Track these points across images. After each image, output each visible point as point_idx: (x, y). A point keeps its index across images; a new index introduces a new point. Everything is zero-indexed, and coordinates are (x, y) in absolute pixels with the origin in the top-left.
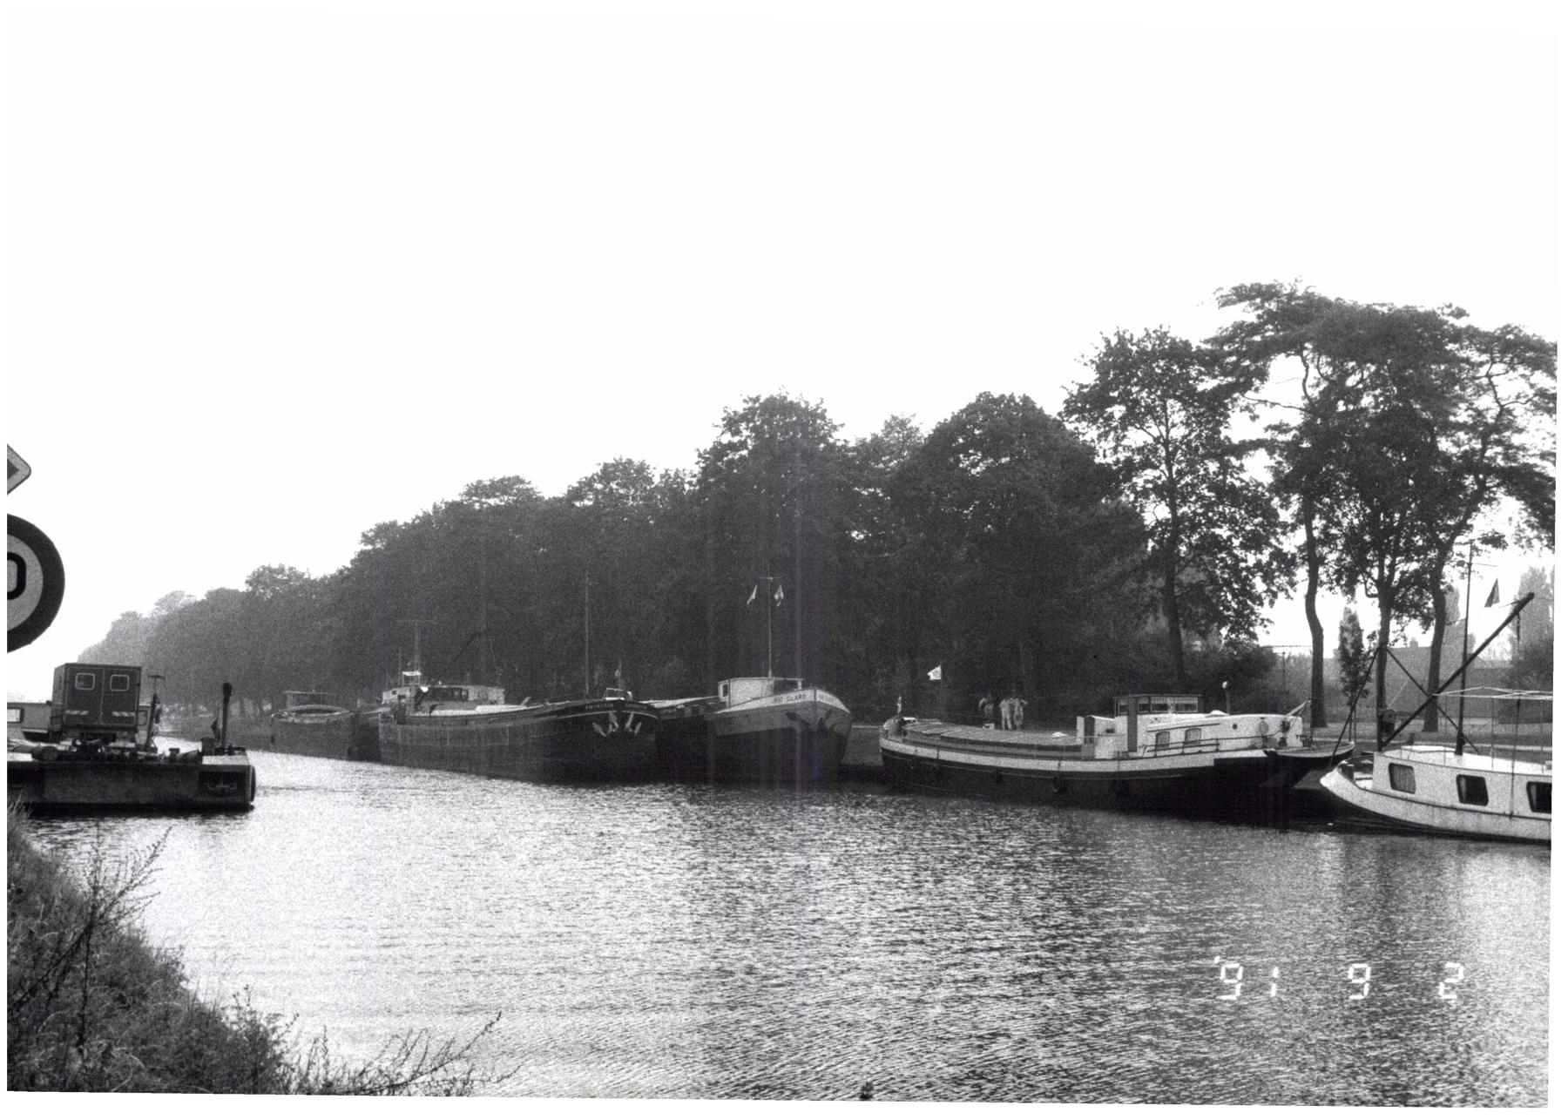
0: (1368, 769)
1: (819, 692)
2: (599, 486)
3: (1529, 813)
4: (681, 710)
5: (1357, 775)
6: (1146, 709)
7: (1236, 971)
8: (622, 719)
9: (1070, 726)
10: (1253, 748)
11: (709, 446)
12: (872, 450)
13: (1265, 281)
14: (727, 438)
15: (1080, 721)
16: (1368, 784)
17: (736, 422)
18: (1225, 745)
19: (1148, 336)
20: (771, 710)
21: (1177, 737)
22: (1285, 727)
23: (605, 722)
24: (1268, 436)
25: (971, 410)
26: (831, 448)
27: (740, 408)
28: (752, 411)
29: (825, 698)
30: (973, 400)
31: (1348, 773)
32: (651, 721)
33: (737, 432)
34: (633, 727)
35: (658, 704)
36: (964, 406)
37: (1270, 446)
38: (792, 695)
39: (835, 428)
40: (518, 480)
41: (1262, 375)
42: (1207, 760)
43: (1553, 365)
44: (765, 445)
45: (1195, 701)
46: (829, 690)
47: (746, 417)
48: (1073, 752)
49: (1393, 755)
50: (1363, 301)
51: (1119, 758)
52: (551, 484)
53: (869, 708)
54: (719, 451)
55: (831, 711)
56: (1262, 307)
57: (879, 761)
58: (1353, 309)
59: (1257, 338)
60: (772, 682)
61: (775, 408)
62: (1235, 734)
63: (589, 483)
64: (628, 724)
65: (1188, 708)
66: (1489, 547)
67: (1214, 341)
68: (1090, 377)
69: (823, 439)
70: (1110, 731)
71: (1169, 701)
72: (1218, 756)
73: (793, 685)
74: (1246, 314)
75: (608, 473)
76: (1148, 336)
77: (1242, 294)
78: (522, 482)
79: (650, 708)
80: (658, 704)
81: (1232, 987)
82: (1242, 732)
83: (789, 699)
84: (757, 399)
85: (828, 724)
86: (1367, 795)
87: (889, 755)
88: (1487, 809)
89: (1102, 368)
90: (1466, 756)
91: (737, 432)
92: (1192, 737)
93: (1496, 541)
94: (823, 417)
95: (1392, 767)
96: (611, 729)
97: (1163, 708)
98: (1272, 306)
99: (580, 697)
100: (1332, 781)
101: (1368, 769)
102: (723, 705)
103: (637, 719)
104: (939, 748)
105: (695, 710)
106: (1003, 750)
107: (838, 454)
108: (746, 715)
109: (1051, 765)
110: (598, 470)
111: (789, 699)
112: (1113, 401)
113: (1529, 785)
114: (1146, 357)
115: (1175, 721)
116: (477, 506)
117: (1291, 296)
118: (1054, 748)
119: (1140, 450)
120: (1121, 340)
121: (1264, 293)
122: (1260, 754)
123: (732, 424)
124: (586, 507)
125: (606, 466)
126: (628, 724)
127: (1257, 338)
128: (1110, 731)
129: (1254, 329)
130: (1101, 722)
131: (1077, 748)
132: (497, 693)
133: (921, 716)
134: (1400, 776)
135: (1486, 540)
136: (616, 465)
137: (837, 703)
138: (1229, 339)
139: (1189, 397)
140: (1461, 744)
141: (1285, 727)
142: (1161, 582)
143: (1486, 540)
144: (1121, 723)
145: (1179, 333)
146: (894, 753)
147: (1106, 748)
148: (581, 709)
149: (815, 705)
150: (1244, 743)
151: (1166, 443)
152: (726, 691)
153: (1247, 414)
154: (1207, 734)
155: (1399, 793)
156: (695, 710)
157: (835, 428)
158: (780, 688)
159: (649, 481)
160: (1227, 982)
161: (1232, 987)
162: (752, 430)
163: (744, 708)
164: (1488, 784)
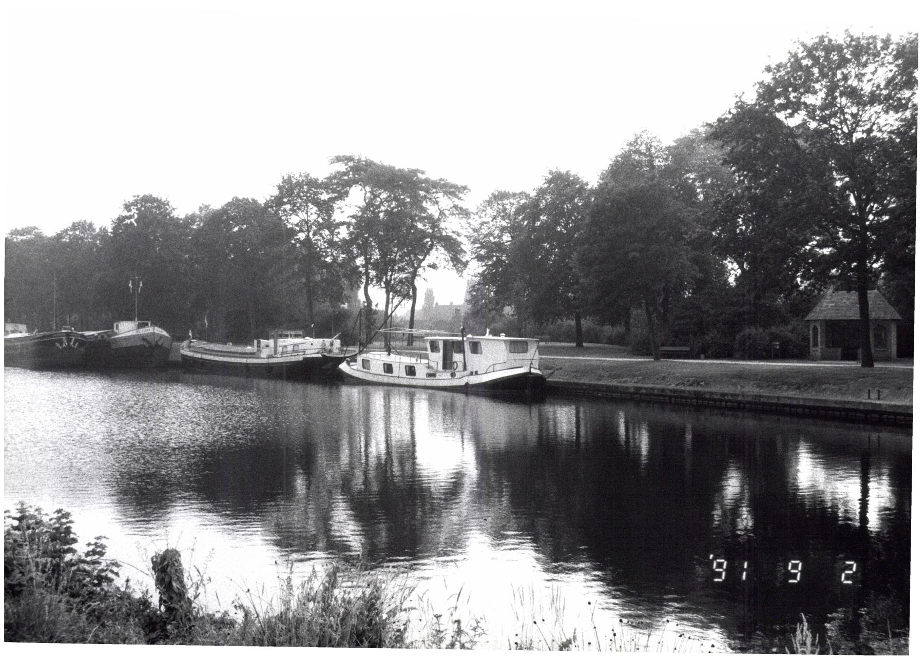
0: (355, 361)
1: (156, 328)
2: (70, 233)
3: (383, 373)
4: (97, 337)
5: (351, 364)
6: (281, 336)
7: (797, 564)
8: (69, 340)
9: (252, 345)
10: (318, 353)
11: (116, 217)
12: (191, 219)
13: (348, 154)
14: (125, 213)
15: (255, 341)
16: (355, 367)
17: (130, 206)
18: (308, 352)
19: (300, 176)
20: (134, 336)
21: (290, 348)
22: (332, 344)
23: (61, 343)
24: (347, 220)
25: (229, 204)
26: (172, 219)
27: (131, 200)
28: (136, 201)
29: (158, 330)
30: (230, 200)
31: (348, 363)
32: (83, 341)
33: (130, 211)
34: (74, 344)
35: (87, 333)
36: (226, 203)
37: (348, 225)
38: (144, 329)
39: (174, 209)
40: (35, 228)
41: (347, 193)
42: (300, 358)
43: (241, 201)
44: (142, 217)
45: (301, 333)
46: (160, 327)
47: (134, 204)
48: (252, 355)
49: (364, 356)
50: (386, 163)
51: (270, 357)
52: (49, 232)
53: (180, 337)
54: (121, 219)
55: (161, 337)
56: (347, 165)
57: (180, 359)
58: (383, 167)
59: (346, 178)
60: (137, 323)
61: (147, 199)
62: (312, 347)
63: (66, 231)
64: (72, 343)
65: (296, 336)
66: (431, 269)
67: (327, 178)
68: (276, 192)
69: (169, 214)
70: (267, 346)
71: (289, 333)
72: (305, 356)
73: (147, 325)
74: (342, 167)
75: (74, 227)
76: (300, 176)
77: (338, 159)
78: (37, 229)
79: (82, 336)
80: (87, 333)
81: (796, 575)
82: (314, 347)
83: (143, 331)
84: (138, 196)
85: (160, 343)
86: (355, 372)
87: (184, 356)
88: (393, 375)
89: (280, 188)
90: (392, 355)
91: (130, 211)
92: (296, 348)
93: (433, 266)
94: (168, 204)
95: (363, 360)
96: (64, 345)
97: (287, 336)
98: (351, 164)
99: (51, 330)
100: (343, 367)
101: (355, 361)
102: (116, 334)
103: (76, 341)
104: (202, 353)
105: (102, 337)
106: (226, 354)
107: (175, 222)
108: (126, 339)
109: (244, 361)
110: (70, 225)
111: (143, 331)
112: (285, 204)
113: (406, 366)
114: (299, 184)
115: (291, 341)
116: (15, 240)
117: (359, 161)
118: (246, 353)
119: (297, 225)
120: (290, 178)
121: (350, 159)
122: (320, 355)
123: (127, 207)
124: (824, 255)
125: (74, 223)
126: (72, 343)
127: (346, 178)
128: (267, 346)
129: (345, 174)
130: (263, 342)
131: (254, 354)
132: (23, 327)
133: (200, 339)
134: (365, 363)
135: (429, 266)
136: (79, 223)
137: (165, 333)
138: (335, 177)
139: (317, 203)
140: (389, 350)
141: (332, 344)
142: (304, 280)
143: (429, 266)
144: (271, 342)
145: (313, 176)
146: (186, 356)
147: (265, 353)
148: (51, 336)
149: (154, 334)
150: (317, 351)
151: (307, 222)
152: (117, 327)
153: (339, 210)
154: (301, 347)
155: (365, 370)
156: (102, 337)
157: (174, 209)
158: (140, 326)
159: (94, 230)
160: (793, 571)
161: (796, 575)
162: (137, 210)
163: (123, 335)
164: (416, 368)
